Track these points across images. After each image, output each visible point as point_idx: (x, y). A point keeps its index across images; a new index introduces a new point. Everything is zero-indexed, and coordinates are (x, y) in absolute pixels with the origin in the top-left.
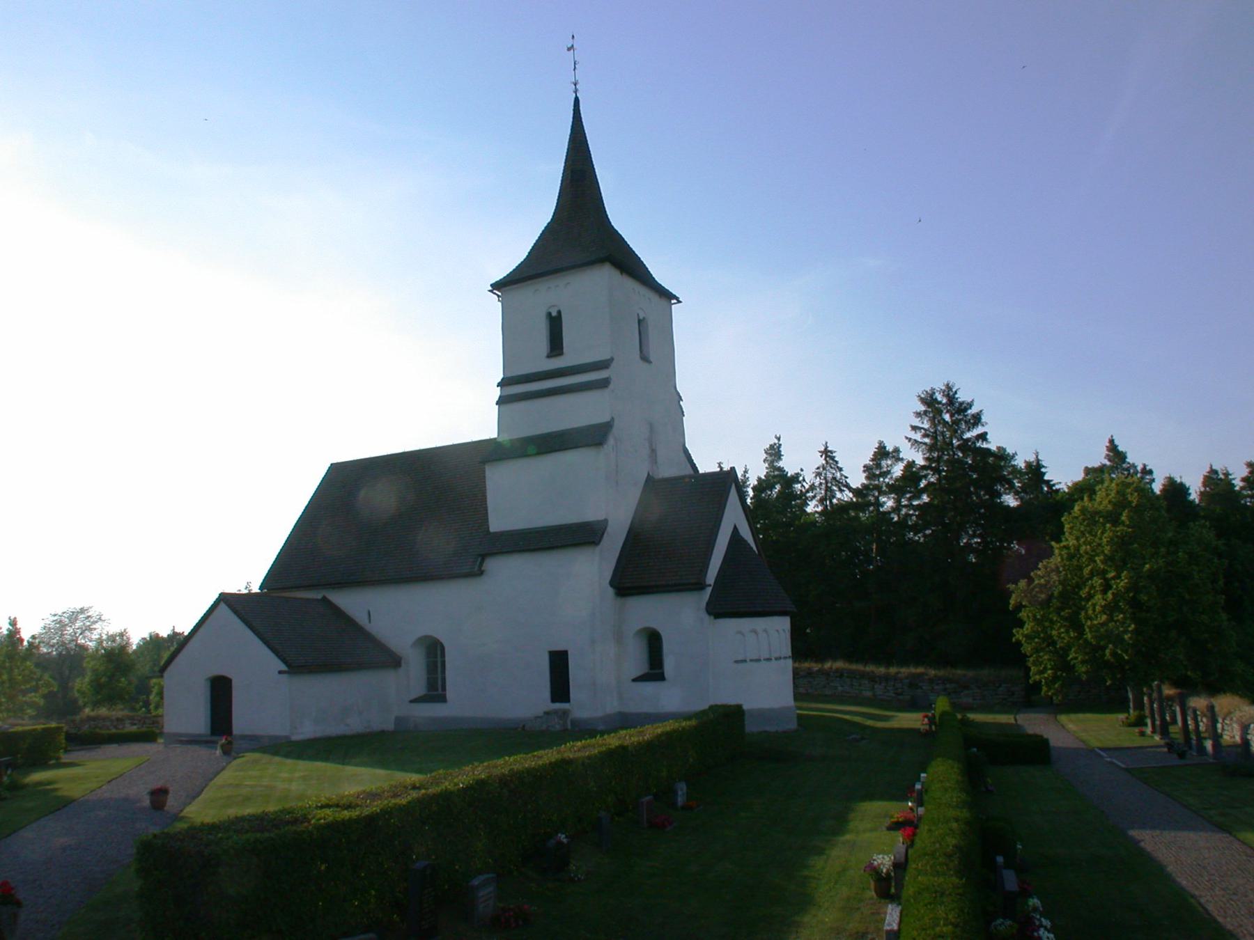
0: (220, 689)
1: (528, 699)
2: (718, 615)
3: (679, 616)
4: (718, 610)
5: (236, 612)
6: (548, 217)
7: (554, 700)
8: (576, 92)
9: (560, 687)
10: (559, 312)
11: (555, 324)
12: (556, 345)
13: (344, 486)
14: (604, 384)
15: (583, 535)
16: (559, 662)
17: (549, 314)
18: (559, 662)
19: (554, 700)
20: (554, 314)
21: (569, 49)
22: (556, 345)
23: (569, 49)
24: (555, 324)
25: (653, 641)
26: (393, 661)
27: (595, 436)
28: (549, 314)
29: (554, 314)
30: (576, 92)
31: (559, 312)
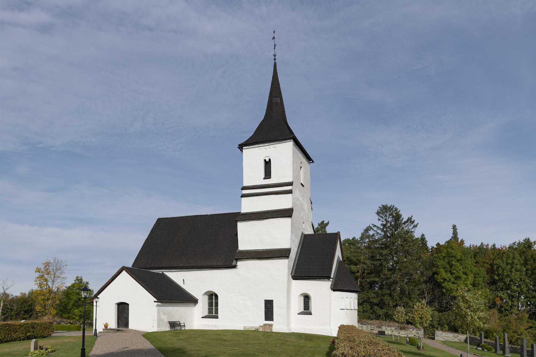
0: (123, 309)
1: (255, 320)
2: (334, 290)
3: (319, 289)
4: (335, 288)
5: (292, 133)
6: (262, 118)
7: (266, 319)
9: (269, 314)
10: (270, 160)
11: (268, 164)
12: (268, 174)
13: (159, 220)
14: (290, 192)
15: (283, 254)
16: (269, 305)
17: (265, 160)
18: (269, 305)
19: (266, 319)
20: (267, 160)
22: (268, 174)
24: (268, 164)
25: (307, 298)
26: (192, 300)
27: (287, 213)
28: (265, 160)
29: (267, 160)
31: (270, 160)
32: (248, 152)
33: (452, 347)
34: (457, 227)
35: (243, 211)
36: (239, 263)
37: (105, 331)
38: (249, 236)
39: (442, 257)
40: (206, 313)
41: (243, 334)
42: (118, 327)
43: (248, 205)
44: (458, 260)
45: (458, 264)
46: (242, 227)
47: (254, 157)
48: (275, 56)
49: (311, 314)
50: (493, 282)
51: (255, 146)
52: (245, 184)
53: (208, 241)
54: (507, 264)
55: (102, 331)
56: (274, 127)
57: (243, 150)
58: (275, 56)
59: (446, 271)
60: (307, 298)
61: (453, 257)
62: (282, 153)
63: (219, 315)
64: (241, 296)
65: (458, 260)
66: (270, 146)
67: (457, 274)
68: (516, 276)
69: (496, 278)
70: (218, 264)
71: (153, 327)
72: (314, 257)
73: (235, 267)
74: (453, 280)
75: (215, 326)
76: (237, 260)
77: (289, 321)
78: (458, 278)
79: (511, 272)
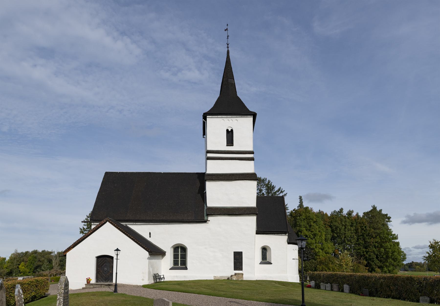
1: (226, 270)
6: (218, 95)
8: (228, 47)
12: (230, 142)
17: (227, 130)
19: (235, 269)
20: (230, 130)
21: (225, 30)
22: (230, 142)
23: (225, 30)
24: (230, 134)
28: (227, 130)
29: (230, 130)
30: (228, 47)
31: (232, 130)
32: (211, 120)
33: (280, 284)
34: (303, 198)
35: (209, 171)
36: (210, 218)
37: (88, 286)
38: (217, 194)
39: (302, 220)
40: (172, 265)
41: (259, 284)
42: (97, 281)
43: (214, 167)
44: (314, 222)
45: (315, 224)
46: (210, 186)
47: (218, 126)
48: (228, 45)
49: (271, 264)
50: (333, 238)
51: (219, 117)
52: (209, 148)
53: (180, 197)
54: (342, 225)
55: (84, 286)
56: (229, 103)
57: (207, 119)
58: (228, 45)
59: (307, 230)
60: (265, 250)
61: (311, 219)
62: (242, 126)
63: (189, 265)
64: (215, 247)
65: (314, 222)
66: (232, 119)
67: (314, 232)
68: (348, 234)
69: (335, 235)
70: (164, 218)
71: (143, 280)
72: (271, 214)
73: (205, 222)
74: (312, 236)
75: (185, 276)
76: (208, 215)
77: (254, 271)
78: (315, 235)
79: (345, 231)
